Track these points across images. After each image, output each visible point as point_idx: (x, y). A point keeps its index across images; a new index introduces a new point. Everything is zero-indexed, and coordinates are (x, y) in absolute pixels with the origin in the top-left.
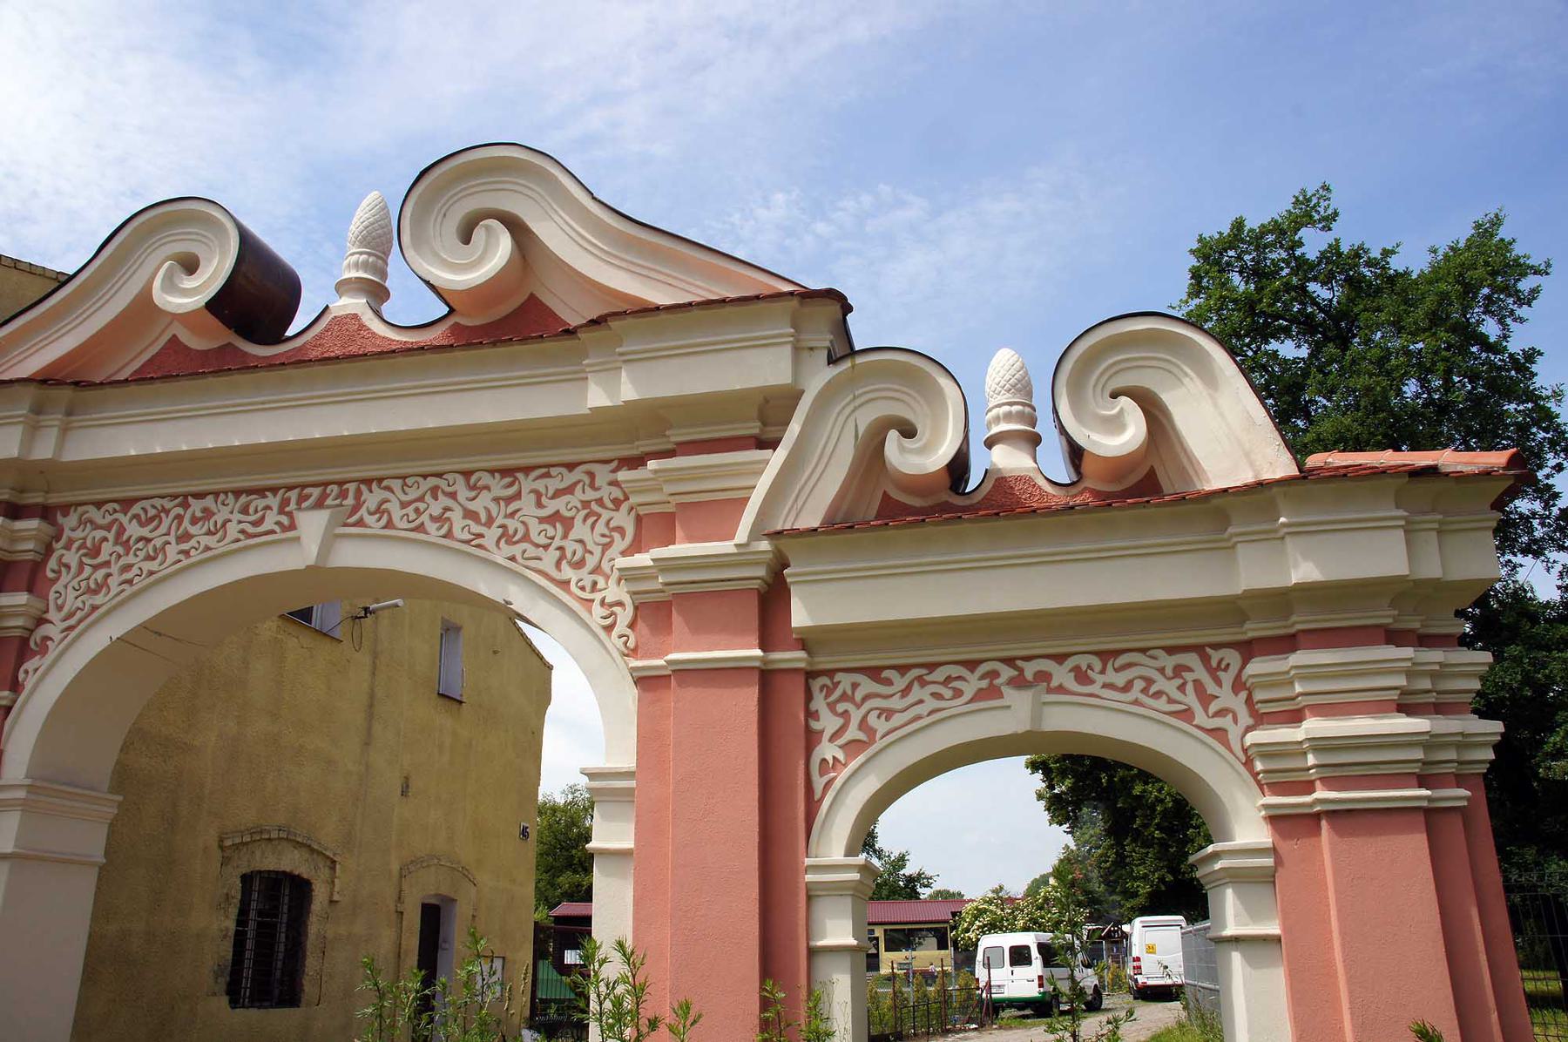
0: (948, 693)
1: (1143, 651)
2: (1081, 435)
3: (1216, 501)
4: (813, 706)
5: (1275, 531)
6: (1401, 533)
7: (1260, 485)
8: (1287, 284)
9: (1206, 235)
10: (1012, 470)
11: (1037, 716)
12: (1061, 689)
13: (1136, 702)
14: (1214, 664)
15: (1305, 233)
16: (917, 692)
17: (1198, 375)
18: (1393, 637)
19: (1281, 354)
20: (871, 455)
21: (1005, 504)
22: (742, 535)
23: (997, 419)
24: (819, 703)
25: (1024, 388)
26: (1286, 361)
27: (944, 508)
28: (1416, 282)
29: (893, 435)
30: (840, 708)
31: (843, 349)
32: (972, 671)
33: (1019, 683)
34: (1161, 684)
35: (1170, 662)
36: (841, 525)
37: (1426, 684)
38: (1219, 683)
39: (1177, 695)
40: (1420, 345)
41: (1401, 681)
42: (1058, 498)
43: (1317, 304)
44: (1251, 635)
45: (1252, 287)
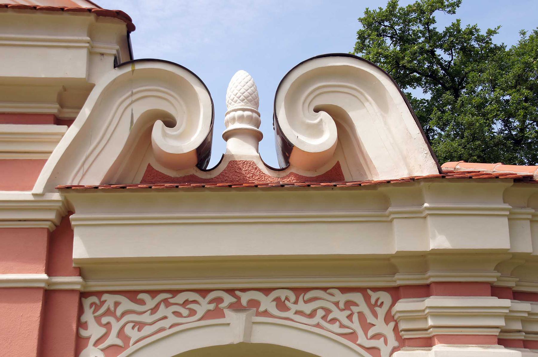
0: (185, 312)
1: (325, 289)
2: (292, 136)
3: (382, 189)
4: (84, 319)
5: (421, 212)
6: (506, 220)
7: (413, 180)
8: (422, 48)
9: (371, 9)
10: (240, 157)
11: (248, 332)
12: (266, 313)
13: (318, 325)
14: (373, 301)
15: (438, 14)
16: (162, 311)
17: (374, 100)
18: (497, 291)
19: (413, 96)
20: (142, 137)
21: (234, 180)
22: (39, 186)
23: (233, 120)
24: (88, 316)
25: (253, 100)
26: (415, 101)
27: (192, 179)
28: (508, 54)
29: (159, 125)
30: (104, 320)
31: (125, 58)
32: (204, 297)
33: (237, 307)
34: (336, 313)
35: (342, 298)
36: (115, 186)
37: (518, 326)
38: (375, 315)
39: (346, 322)
40: (507, 97)
41: (501, 322)
42: (272, 178)
43: (441, 64)
44: (399, 283)
45: (398, 48)
